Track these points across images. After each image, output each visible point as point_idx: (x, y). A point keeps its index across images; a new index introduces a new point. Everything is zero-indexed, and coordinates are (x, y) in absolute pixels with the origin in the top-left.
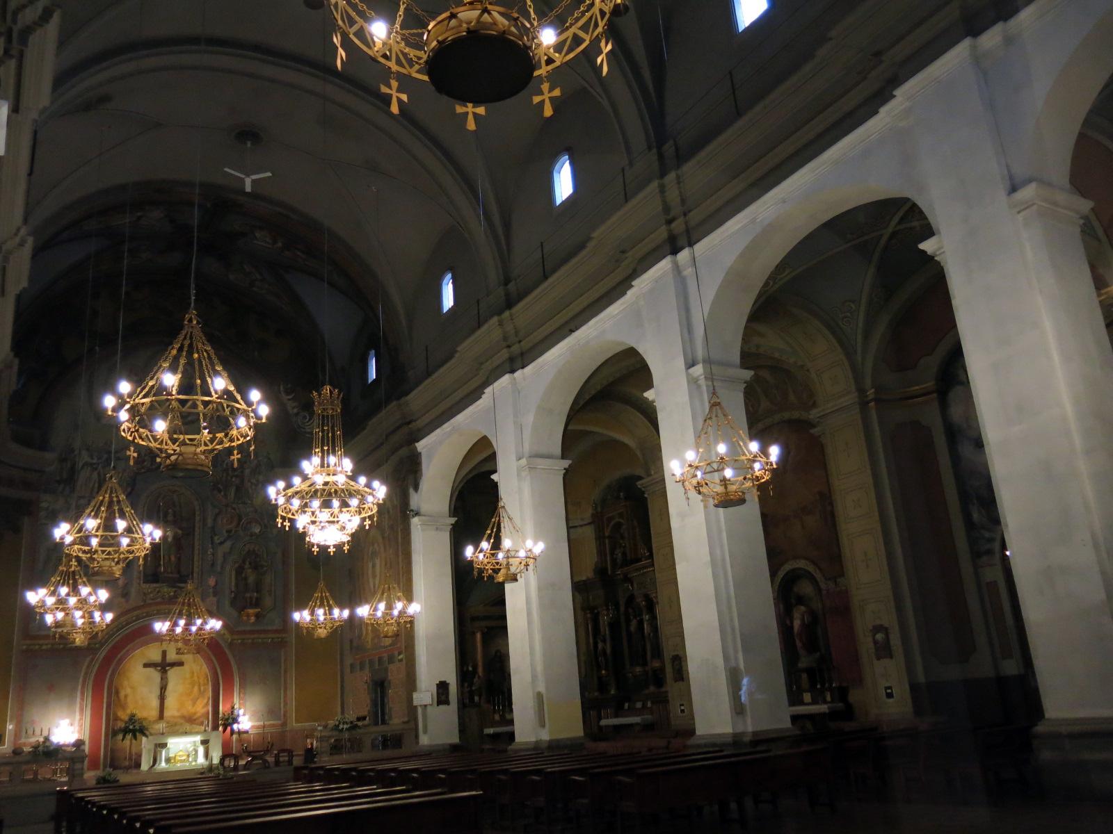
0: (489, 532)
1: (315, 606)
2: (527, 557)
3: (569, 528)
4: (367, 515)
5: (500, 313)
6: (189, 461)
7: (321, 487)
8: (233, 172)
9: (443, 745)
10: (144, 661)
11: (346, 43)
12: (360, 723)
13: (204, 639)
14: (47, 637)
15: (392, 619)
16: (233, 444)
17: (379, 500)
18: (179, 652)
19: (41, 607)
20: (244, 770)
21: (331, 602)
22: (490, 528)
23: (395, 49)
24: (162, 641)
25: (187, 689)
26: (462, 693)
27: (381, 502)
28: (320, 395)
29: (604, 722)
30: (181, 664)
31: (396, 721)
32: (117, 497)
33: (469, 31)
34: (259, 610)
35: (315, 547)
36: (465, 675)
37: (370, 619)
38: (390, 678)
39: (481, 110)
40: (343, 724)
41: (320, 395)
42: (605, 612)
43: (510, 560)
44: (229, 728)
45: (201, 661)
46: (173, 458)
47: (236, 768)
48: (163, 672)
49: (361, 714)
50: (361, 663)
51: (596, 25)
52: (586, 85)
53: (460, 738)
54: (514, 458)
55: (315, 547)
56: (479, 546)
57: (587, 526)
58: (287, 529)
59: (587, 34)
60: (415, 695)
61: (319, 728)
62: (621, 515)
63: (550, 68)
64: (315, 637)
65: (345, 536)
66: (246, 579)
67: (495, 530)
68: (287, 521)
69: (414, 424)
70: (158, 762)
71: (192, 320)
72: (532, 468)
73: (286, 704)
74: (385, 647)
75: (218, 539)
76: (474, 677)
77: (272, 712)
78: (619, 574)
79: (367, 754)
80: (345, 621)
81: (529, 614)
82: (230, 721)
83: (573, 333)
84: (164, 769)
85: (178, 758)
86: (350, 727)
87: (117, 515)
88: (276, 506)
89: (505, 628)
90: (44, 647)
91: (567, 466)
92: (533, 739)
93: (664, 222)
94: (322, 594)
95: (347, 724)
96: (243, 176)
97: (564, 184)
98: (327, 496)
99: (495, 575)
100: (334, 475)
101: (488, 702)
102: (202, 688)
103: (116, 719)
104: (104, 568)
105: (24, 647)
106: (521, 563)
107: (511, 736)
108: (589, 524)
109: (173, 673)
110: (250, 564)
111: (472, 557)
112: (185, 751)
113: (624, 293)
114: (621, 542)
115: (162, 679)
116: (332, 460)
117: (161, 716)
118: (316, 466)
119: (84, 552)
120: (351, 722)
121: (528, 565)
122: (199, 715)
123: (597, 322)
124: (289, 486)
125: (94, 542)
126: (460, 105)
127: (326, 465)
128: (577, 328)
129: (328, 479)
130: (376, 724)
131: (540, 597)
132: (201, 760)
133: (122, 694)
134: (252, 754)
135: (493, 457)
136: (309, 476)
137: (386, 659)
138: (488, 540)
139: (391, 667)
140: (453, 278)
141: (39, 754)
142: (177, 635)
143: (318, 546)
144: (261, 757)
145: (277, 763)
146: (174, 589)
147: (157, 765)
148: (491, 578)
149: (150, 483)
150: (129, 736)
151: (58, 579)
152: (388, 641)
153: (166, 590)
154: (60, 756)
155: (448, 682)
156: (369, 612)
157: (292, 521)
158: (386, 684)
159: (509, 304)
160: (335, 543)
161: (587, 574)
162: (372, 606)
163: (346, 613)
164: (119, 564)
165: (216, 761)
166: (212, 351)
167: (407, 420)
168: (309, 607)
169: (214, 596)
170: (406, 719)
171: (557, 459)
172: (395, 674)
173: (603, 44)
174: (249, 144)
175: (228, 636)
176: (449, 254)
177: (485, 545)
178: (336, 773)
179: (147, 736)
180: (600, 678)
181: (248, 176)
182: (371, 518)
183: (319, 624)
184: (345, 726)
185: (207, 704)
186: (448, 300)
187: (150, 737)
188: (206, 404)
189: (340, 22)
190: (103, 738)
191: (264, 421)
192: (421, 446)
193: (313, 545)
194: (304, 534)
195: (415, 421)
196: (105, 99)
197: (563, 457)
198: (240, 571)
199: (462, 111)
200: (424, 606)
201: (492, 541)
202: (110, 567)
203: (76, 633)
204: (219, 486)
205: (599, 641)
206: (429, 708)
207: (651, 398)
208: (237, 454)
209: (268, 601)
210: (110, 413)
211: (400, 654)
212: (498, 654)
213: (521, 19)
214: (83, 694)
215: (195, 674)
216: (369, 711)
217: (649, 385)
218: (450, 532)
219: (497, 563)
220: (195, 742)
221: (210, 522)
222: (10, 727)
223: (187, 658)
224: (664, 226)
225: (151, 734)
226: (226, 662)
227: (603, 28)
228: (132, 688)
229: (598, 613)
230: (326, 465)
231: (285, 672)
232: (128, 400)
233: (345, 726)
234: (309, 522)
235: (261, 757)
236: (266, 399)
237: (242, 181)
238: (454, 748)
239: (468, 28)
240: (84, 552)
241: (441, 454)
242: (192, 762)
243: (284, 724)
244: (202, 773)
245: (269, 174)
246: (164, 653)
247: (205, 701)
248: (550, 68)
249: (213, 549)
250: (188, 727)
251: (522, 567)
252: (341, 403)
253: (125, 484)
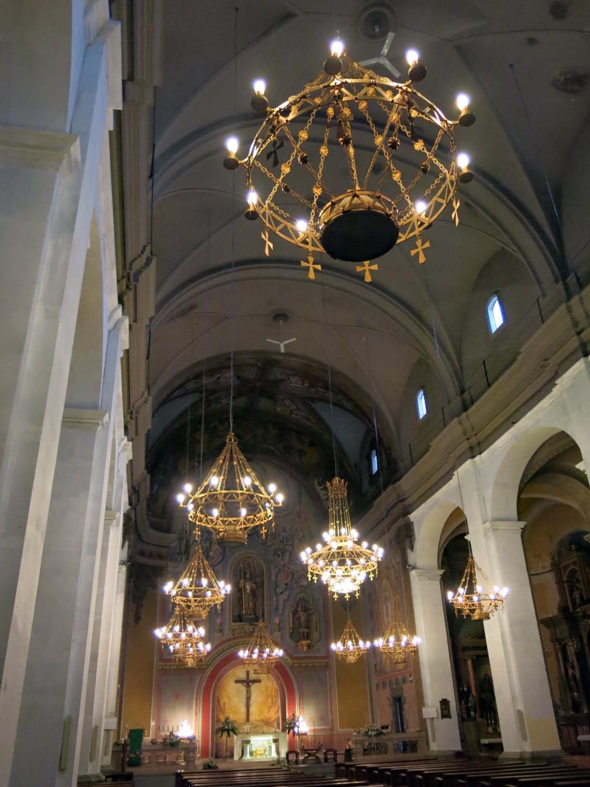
0: (463, 580)
1: (345, 639)
2: (495, 600)
3: (530, 576)
4: (371, 570)
5: (459, 415)
6: (231, 536)
7: (336, 550)
8: (271, 341)
9: (449, 751)
10: (235, 679)
11: (273, 237)
12: (384, 731)
13: (272, 663)
14: (170, 660)
15: (401, 649)
16: (262, 523)
17: (378, 558)
18: (256, 672)
19: (165, 639)
20: (303, 764)
21: (357, 636)
22: (464, 577)
23: (311, 236)
24: (245, 664)
25: (263, 700)
26: (461, 709)
27: (380, 560)
28: (332, 484)
29: (581, 738)
30: (259, 681)
31: (412, 730)
32: (203, 563)
33: (344, 212)
34: (309, 641)
35: (336, 595)
36: (462, 695)
37: (384, 649)
38: (405, 695)
39: (375, 267)
40: (372, 731)
41: (332, 484)
42: (571, 644)
43: (482, 602)
44: (292, 731)
45: (272, 679)
46: (221, 534)
47: (297, 762)
48: (247, 687)
49: (386, 724)
50: (383, 683)
51: (449, 192)
52: (505, 246)
53: (462, 746)
54: (480, 522)
55: (336, 595)
56: (457, 591)
57: (548, 573)
58: (315, 582)
59: (444, 199)
60: (424, 710)
61: (354, 734)
62: (574, 563)
63: (421, 228)
64: (347, 662)
65: (356, 586)
66: (299, 618)
67: (468, 579)
68: (315, 576)
69: (406, 501)
70: (245, 755)
71: (231, 440)
72: (495, 530)
73: (332, 713)
74: (399, 671)
75: (279, 590)
76: (469, 696)
77: (322, 718)
78: (579, 612)
79: (391, 756)
80: (368, 650)
81: (504, 643)
82: (292, 725)
83: (515, 425)
84: (249, 760)
85: (258, 752)
86: (377, 734)
87: (203, 575)
88: (307, 565)
89: (487, 656)
90: (172, 668)
91: (523, 527)
92: (518, 750)
93: (575, 334)
94: (350, 629)
95: (374, 731)
96: (279, 343)
97: (496, 317)
98: (341, 557)
99: (471, 614)
100: (345, 541)
101: (482, 716)
102: (274, 699)
103: (218, 721)
104: (196, 612)
105: (160, 667)
106: (491, 604)
107: (500, 747)
108: (550, 571)
109: (254, 687)
110: (301, 607)
111: (452, 600)
112: (263, 748)
113: (550, 391)
114: (578, 585)
115: (247, 692)
116: (343, 530)
117: (248, 720)
118: (332, 535)
119: (184, 601)
120: (377, 730)
121: (497, 606)
122: (273, 719)
123: (532, 415)
124: (314, 550)
125: (190, 594)
126: (359, 265)
127: (339, 534)
128: (518, 421)
129: (340, 544)
130: (398, 731)
131: (512, 632)
132: (274, 755)
133: (222, 702)
134: (308, 752)
135: (464, 524)
136: (328, 543)
137: (401, 680)
138: (463, 587)
139: (405, 686)
140: (425, 394)
141: (167, 745)
142: (254, 660)
143: (338, 594)
144: (313, 755)
145: (326, 760)
146: (252, 627)
147: (244, 756)
148: (469, 616)
149: (221, 553)
150: (225, 734)
151: (174, 620)
152: (401, 666)
153: (247, 627)
154: (180, 746)
155: (448, 699)
156: (383, 643)
157: (318, 576)
158: (402, 700)
159: (465, 408)
160: (349, 592)
161: (553, 611)
162: (384, 639)
163: (368, 644)
164: (206, 609)
165: (283, 755)
166: (245, 459)
167: (401, 498)
168: (341, 639)
169: (279, 631)
170: (418, 729)
171: (514, 521)
172: (408, 693)
173: (454, 204)
174: (281, 321)
175: (290, 661)
176: (420, 377)
177: (461, 590)
178: (364, 770)
179: (237, 735)
180: (573, 699)
181: (282, 342)
182: (374, 572)
183: (350, 653)
184: (373, 733)
185: (278, 711)
186: (422, 410)
187: (239, 736)
188: (242, 494)
189: (268, 225)
190: (210, 733)
191: (280, 505)
192: (413, 517)
193: (333, 594)
194: (327, 586)
195: (407, 498)
196: (192, 307)
197: (520, 519)
198: (295, 613)
199: (361, 270)
200: (426, 640)
201: (466, 587)
202: (199, 611)
203: (188, 658)
204: (278, 552)
205: (569, 668)
206: (435, 720)
207: (582, 469)
208: (265, 529)
209: (315, 635)
210: (181, 506)
211: (410, 676)
212: (487, 678)
213: (382, 196)
214: (197, 701)
215: (269, 689)
216: (392, 721)
217: (580, 459)
218: (440, 581)
219: (473, 605)
220: (269, 740)
221: (273, 578)
222: (153, 724)
223: (263, 677)
224: (576, 336)
225: (240, 733)
226: (293, 679)
227: (454, 192)
228: (228, 698)
229: (566, 644)
230: (339, 534)
231: (330, 688)
232: (191, 496)
233: (373, 733)
234: (330, 576)
235: (313, 755)
236: (280, 489)
237: (278, 346)
238: (458, 755)
239: (343, 210)
240: (184, 601)
241: (427, 523)
242: (267, 755)
243: (332, 729)
244: (272, 765)
245: (294, 339)
246: (248, 673)
247: (277, 709)
248: (421, 228)
249: (276, 597)
250: (265, 729)
251: (492, 608)
252: (348, 489)
253: (218, 554)
